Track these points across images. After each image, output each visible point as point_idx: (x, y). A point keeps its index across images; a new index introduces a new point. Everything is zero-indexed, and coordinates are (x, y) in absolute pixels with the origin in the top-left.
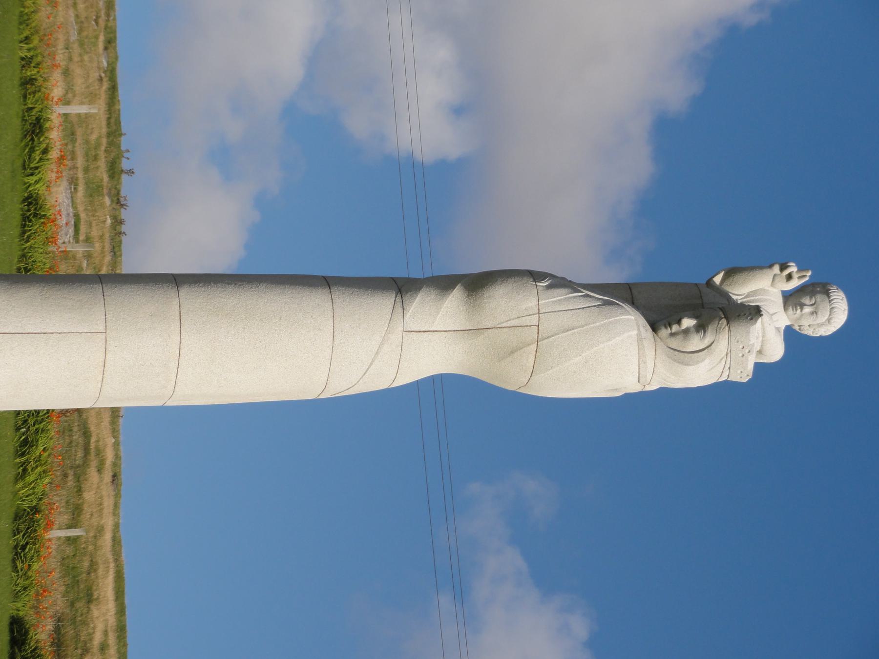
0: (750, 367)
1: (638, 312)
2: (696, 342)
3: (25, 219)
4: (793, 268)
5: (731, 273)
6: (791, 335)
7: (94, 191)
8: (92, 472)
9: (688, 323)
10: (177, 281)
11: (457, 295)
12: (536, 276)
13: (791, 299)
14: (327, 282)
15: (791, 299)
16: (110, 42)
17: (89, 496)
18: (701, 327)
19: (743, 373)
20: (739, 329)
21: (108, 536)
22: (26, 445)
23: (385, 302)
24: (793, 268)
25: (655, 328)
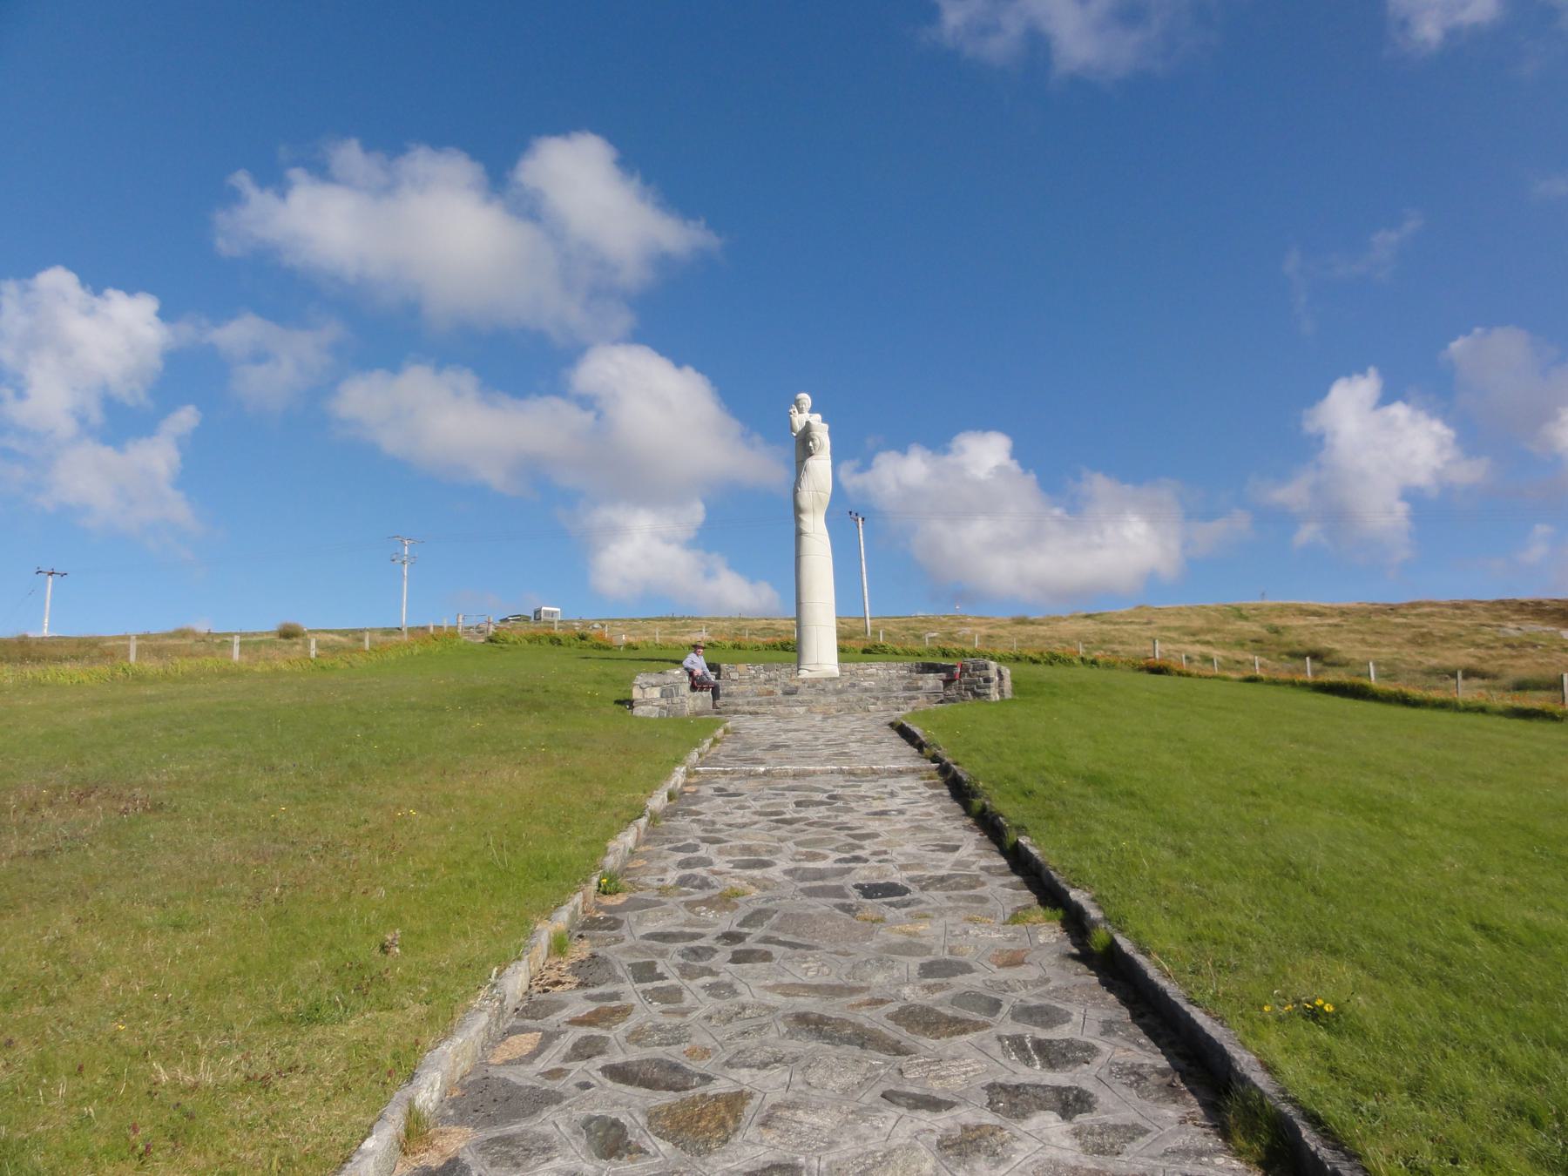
0: (824, 425)
1: (15, 635)
2: (817, 442)
3: (740, 648)
4: (791, 411)
5: (792, 430)
6: (812, 411)
7: (686, 626)
8: (776, 626)
9: (811, 444)
10: (799, 603)
11: (802, 516)
12: (796, 492)
13: (800, 411)
14: (798, 558)
15: (800, 411)
16: (633, 620)
17: (783, 628)
18: (812, 440)
19: (826, 427)
20: (813, 428)
21: (785, 622)
22: (785, 647)
23: (805, 539)
24: (791, 411)
25: (811, 455)
